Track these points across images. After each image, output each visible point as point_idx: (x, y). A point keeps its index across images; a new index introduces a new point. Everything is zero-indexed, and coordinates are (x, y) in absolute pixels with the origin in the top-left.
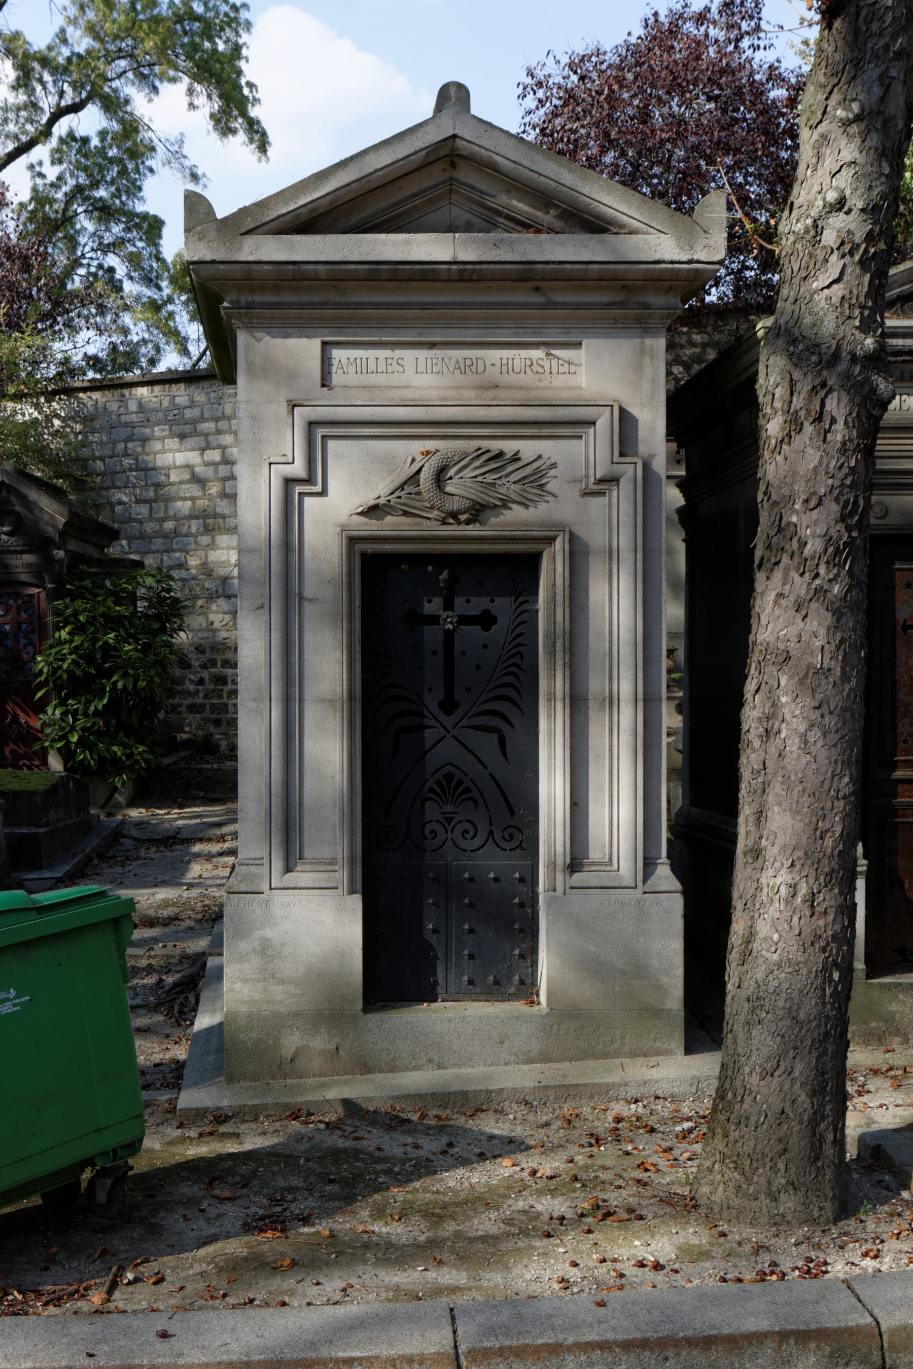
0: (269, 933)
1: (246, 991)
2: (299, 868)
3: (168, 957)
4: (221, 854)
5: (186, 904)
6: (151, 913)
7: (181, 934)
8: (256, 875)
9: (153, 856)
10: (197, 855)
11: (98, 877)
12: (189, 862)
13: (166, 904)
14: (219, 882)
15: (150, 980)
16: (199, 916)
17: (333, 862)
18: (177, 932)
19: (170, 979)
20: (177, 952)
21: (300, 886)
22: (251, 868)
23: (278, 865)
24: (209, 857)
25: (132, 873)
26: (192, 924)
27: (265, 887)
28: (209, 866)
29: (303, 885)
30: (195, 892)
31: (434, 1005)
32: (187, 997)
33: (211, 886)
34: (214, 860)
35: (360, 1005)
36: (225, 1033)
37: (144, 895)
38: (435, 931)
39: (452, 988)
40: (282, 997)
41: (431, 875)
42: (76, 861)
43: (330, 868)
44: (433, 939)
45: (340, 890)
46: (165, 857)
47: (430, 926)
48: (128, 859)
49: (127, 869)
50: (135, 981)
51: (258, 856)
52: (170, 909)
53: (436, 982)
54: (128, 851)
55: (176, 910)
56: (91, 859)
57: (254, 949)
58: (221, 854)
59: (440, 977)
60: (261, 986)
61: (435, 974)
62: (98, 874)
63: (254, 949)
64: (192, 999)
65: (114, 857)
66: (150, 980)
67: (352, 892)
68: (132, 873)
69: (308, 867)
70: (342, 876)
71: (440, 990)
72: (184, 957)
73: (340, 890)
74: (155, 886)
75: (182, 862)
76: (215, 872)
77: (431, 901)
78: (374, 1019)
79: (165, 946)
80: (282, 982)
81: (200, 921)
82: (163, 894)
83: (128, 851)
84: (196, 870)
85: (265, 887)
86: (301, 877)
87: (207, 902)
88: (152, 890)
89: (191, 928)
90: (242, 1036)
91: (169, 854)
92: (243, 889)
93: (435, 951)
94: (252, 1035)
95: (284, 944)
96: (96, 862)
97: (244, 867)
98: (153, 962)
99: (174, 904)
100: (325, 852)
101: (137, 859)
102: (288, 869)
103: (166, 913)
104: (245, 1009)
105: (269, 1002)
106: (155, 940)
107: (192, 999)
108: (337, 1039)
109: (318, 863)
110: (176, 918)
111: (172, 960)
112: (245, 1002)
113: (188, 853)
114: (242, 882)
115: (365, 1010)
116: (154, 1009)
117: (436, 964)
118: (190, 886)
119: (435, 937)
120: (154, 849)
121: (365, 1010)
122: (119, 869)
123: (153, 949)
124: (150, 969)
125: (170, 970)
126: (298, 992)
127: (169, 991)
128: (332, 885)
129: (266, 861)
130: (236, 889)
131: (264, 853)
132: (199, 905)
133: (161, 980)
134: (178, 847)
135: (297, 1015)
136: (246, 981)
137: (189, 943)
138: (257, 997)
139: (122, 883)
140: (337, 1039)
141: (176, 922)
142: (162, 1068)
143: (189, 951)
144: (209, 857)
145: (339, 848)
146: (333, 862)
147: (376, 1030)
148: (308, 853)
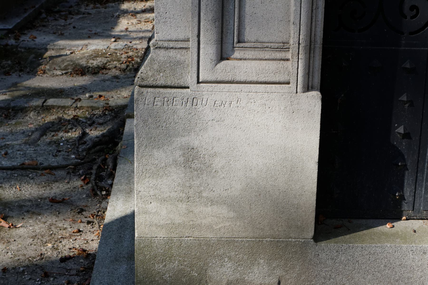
0: (194, 141)
1: (164, 212)
2: (237, 54)
3: (93, 108)
4: (144, 11)
5: (113, 55)
6: (83, 63)
7: (108, 83)
8: (179, 63)
9: (90, 11)
10: (125, 12)
11: (44, 29)
12: (118, 17)
13: (96, 55)
14: (141, 35)
15: (74, 134)
16: (124, 66)
17: (284, 47)
18: (104, 81)
19: (94, 133)
20: (102, 103)
21: (238, 79)
22: (172, 53)
23: (208, 51)
24: (135, 13)
25: (71, 26)
26: (118, 73)
27: (190, 79)
28: (134, 21)
29: (243, 79)
30: (121, 44)
31: (402, 225)
32: (105, 159)
33: (135, 39)
34: (138, 16)
35: (311, 233)
36: (137, 263)
37: (78, 46)
38: (406, 136)
39: (420, 204)
40: (213, 220)
41: (408, 66)
42: (26, 15)
43: (279, 55)
44: (403, 146)
45: (293, 85)
46: (100, 12)
47: (401, 130)
48: (70, 13)
49: (68, 21)
50: (61, 134)
51: (181, 37)
52: (99, 59)
53: (402, 198)
54: (71, 7)
55: (104, 60)
56: (40, 13)
57: (175, 161)
58: (144, 11)
59: (408, 192)
60: (183, 207)
61: (401, 188)
62: (44, 26)
63: (175, 161)
64: (110, 163)
65: (59, 12)
66: (74, 134)
67: (308, 88)
68: (71, 26)
69: (249, 54)
70: (295, 67)
71: (405, 207)
72: (108, 108)
73: (293, 85)
74: (89, 37)
75: (113, 16)
76: (139, 26)
77: (404, 98)
78: (329, 247)
79: (91, 97)
80: (212, 202)
81: (124, 70)
82: (97, 45)
83: (71, 7)
84: (124, 24)
85: (190, 79)
86: (242, 66)
87: (131, 54)
88: (86, 42)
89: (116, 77)
90: (159, 267)
91: (103, 10)
92: (161, 82)
93: (404, 160)
94: (171, 266)
95: (215, 155)
96: (44, 15)
97: (162, 52)
98: (79, 113)
99: (103, 55)
100: (275, 35)
101: (78, 13)
102: (222, 56)
103: (95, 63)
104: (162, 234)
105: (193, 227)
106: (84, 89)
107: (110, 163)
108: (279, 272)
109: (263, 48)
110: (104, 68)
111: (96, 112)
112: (162, 227)
113: (118, 9)
114: (159, 71)
115: (318, 237)
116: (72, 170)
117: (403, 176)
118: (117, 38)
119: (404, 142)
120: (92, 6)
121: (318, 237)
122: (62, 22)
123: (80, 100)
124: (76, 121)
125: (94, 122)
126: (232, 214)
127: (90, 149)
128: (282, 79)
129: (192, 44)
130: (150, 81)
131: (191, 34)
132: (123, 56)
133: (84, 134)
134: (111, 4)
135: (230, 242)
136: (164, 200)
137: (113, 93)
138: (178, 220)
139: (62, 34)
140: (279, 272)
141: (104, 71)
142: (70, 265)
143: (112, 103)
144: (135, 13)
145: (293, 30)
146: (284, 47)
147: (330, 262)
148: (250, 34)
